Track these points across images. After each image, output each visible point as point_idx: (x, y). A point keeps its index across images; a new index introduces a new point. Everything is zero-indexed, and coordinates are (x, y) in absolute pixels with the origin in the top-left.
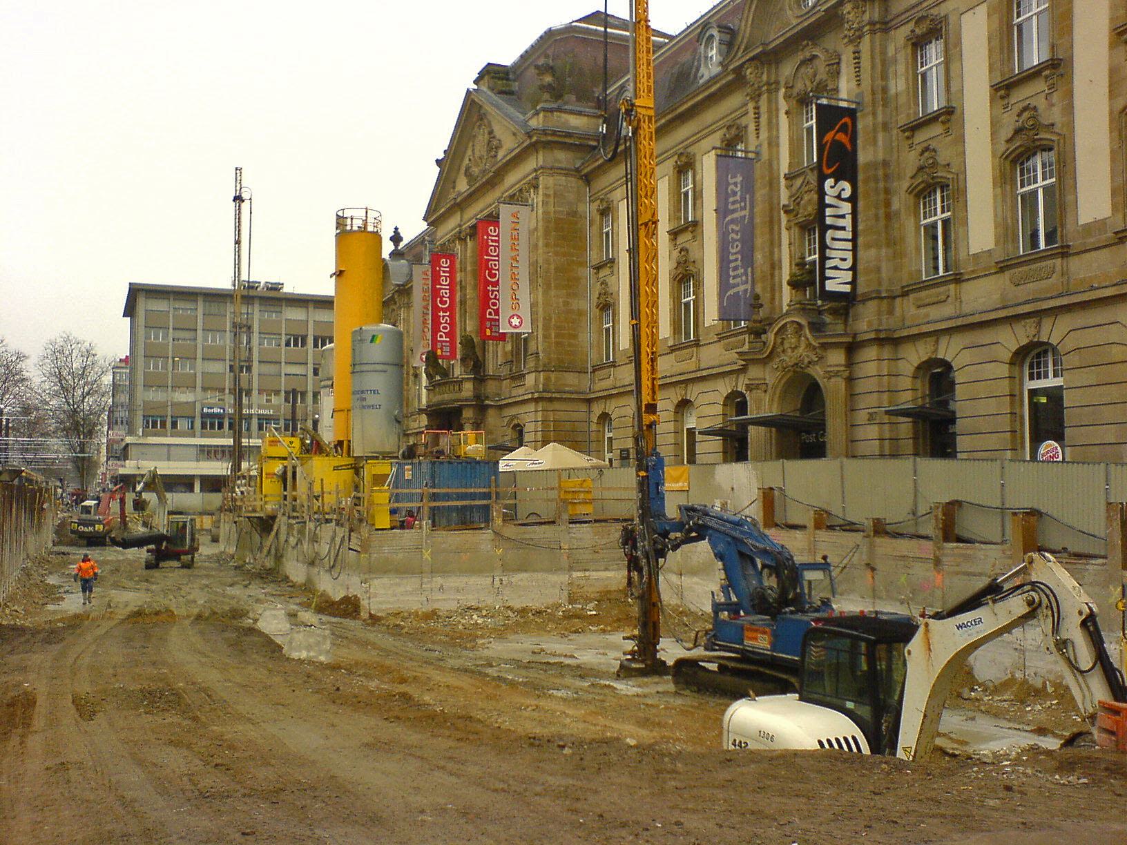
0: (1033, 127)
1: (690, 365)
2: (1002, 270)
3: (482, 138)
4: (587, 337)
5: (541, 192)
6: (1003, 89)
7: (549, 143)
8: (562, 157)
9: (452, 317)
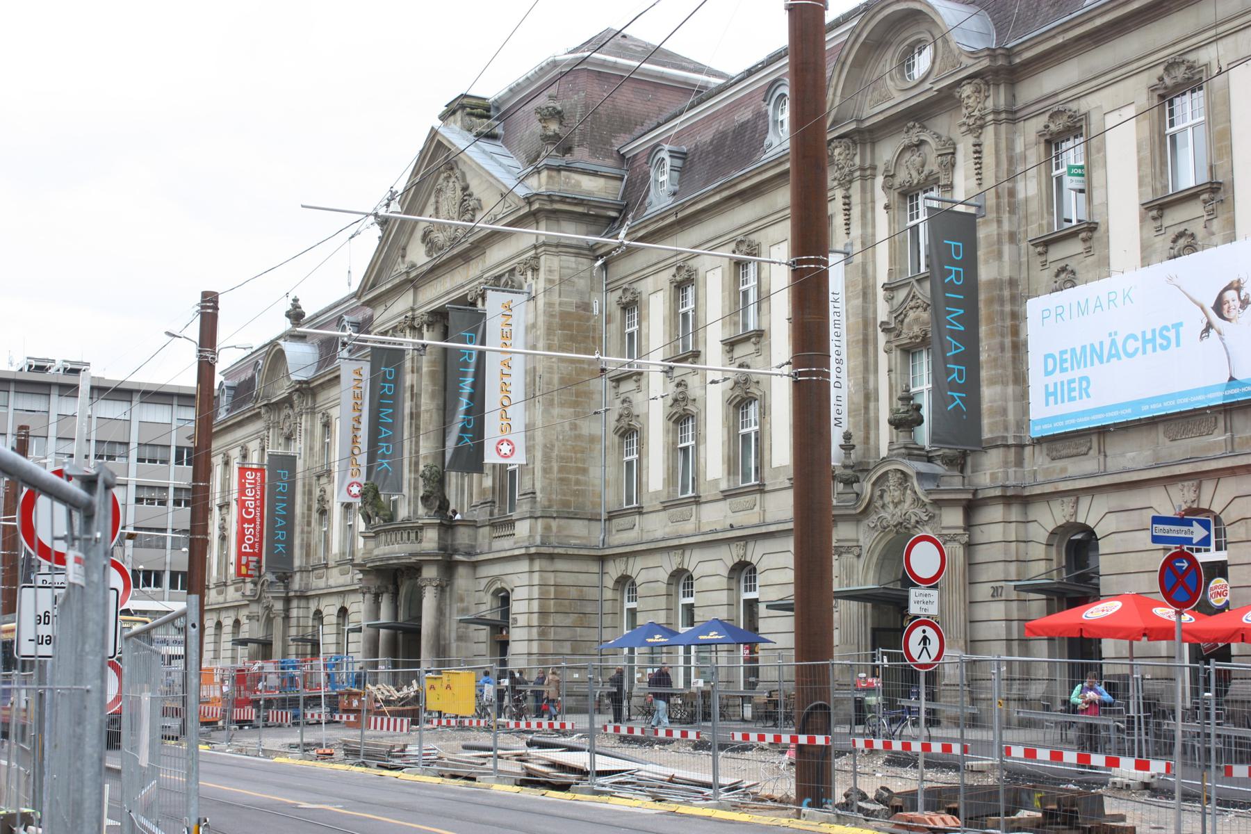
3: (451, 195)
5: (542, 274)
8: (571, 233)
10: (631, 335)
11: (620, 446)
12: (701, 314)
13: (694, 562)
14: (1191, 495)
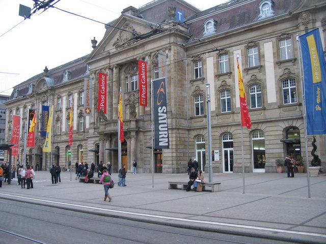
6: (218, 76)
9: (146, 88)
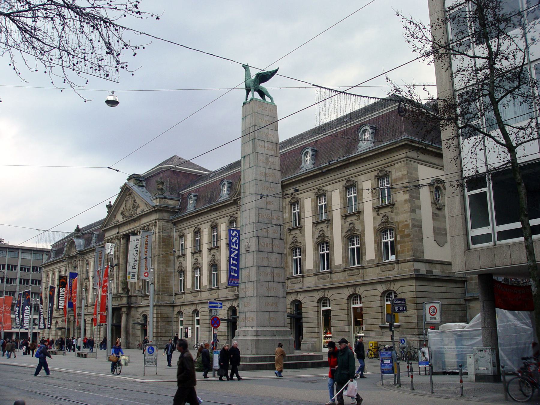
0: (323, 236)
1: (216, 296)
2: (315, 275)
3: (130, 202)
4: (174, 283)
5: (157, 227)
7: (161, 210)
8: (166, 215)
10: (182, 244)
11: (179, 276)
12: (202, 241)
13: (199, 308)
14: (353, 290)
